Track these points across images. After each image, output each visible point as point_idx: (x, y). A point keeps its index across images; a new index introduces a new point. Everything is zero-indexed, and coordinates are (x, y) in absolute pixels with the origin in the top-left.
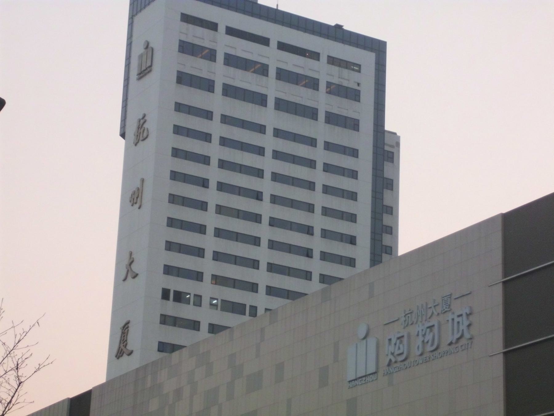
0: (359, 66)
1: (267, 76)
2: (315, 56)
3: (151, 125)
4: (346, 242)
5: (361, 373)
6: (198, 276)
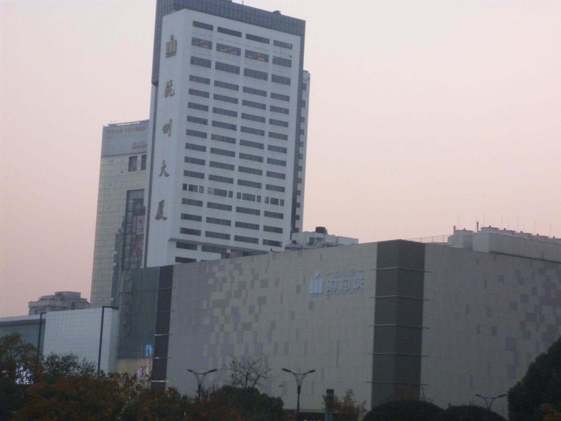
3: (176, 88)
4: (281, 152)
5: (315, 292)
6: (201, 176)
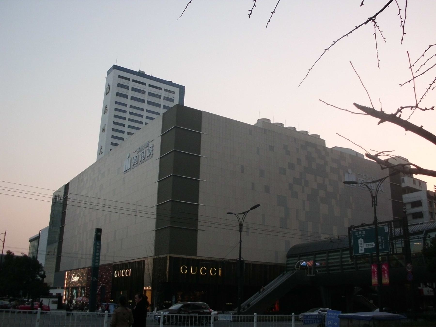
0: (174, 92)
1: (145, 94)
2: (160, 89)
